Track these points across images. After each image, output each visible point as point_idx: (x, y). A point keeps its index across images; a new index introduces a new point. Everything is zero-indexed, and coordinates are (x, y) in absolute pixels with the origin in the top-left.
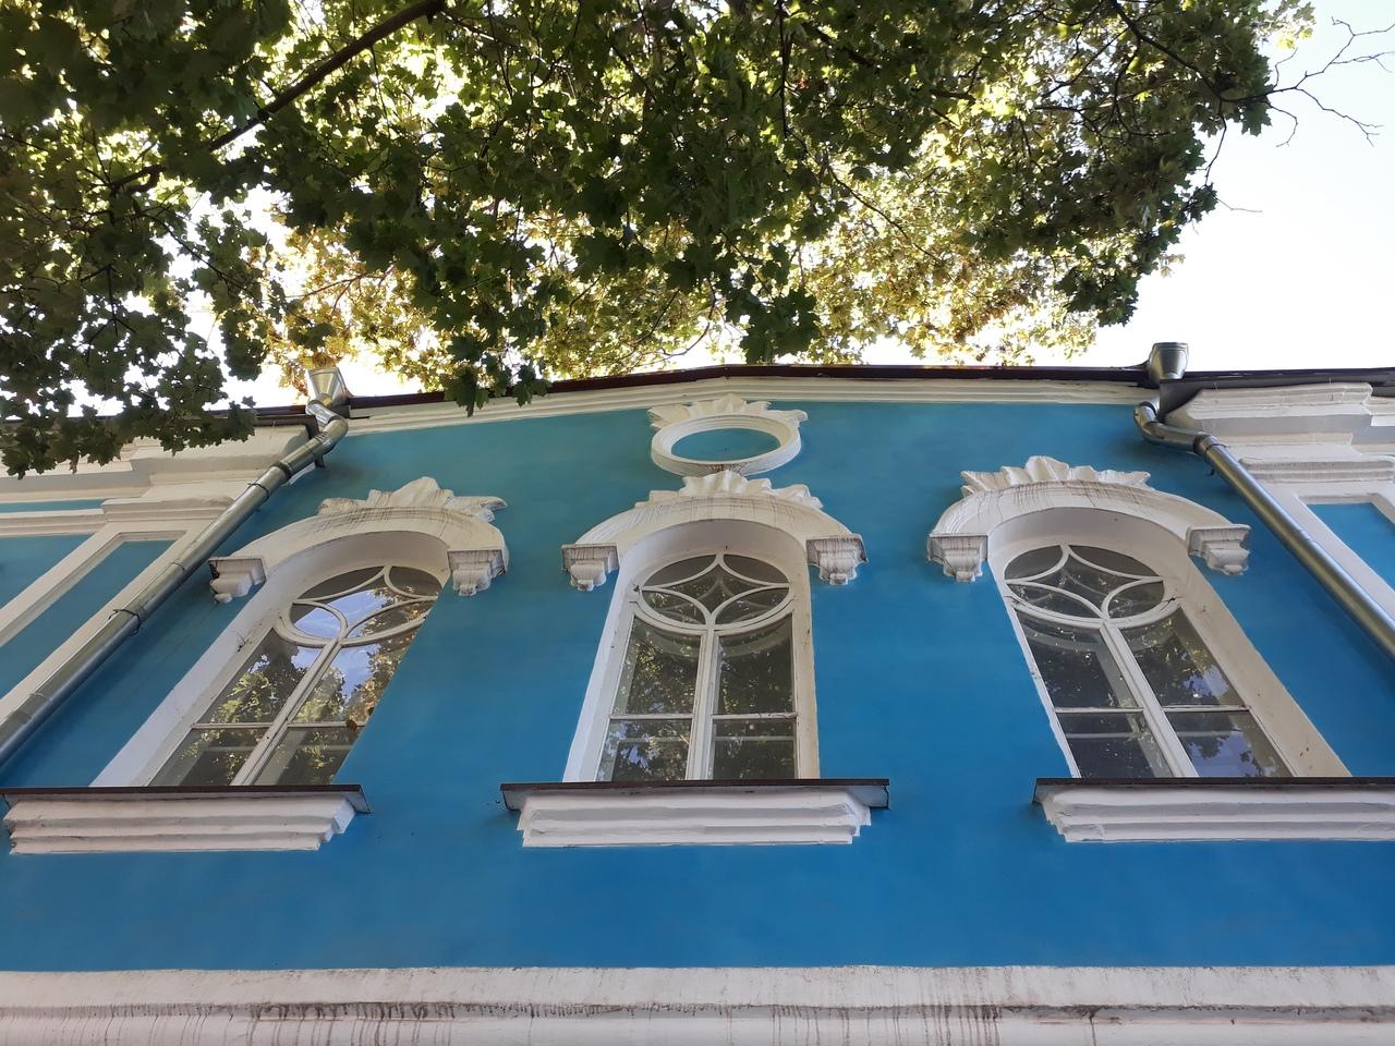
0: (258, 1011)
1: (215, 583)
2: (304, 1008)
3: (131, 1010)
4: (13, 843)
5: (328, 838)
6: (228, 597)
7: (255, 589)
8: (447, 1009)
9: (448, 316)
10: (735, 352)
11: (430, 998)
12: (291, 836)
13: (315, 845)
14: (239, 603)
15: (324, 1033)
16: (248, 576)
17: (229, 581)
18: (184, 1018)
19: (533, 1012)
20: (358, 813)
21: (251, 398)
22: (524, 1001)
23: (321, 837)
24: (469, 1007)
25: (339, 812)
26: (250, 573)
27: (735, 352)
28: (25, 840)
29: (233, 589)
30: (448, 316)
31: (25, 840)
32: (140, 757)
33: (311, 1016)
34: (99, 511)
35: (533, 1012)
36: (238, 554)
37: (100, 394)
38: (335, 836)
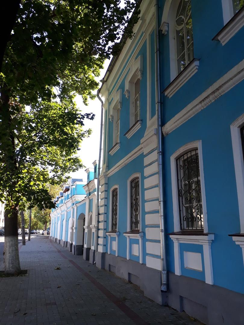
0: (201, 102)
1: (163, 33)
2: (205, 99)
3: (189, 111)
4: (169, 97)
5: (198, 68)
6: (166, 33)
7: (168, 26)
8: (220, 87)
9: (13, 32)
10: (92, 113)
11: (217, 87)
12: (193, 72)
13: (197, 71)
14: (168, 32)
15: (209, 100)
16: (165, 26)
17: (164, 29)
18: (194, 109)
19: (231, 79)
20: (199, 60)
21: (93, 120)
22: (229, 79)
23: (196, 69)
24: (223, 85)
25: (197, 63)
26: (165, 25)
27: (92, 113)
28: (170, 96)
29: (166, 31)
30: (13, 32)
31: (170, 96)
32: (173, 74)
33: (207, 99)
34: (144, 34)
35: (231, 79)
36: (145, 136)
37: (123, 9)
38: (199, 66)
